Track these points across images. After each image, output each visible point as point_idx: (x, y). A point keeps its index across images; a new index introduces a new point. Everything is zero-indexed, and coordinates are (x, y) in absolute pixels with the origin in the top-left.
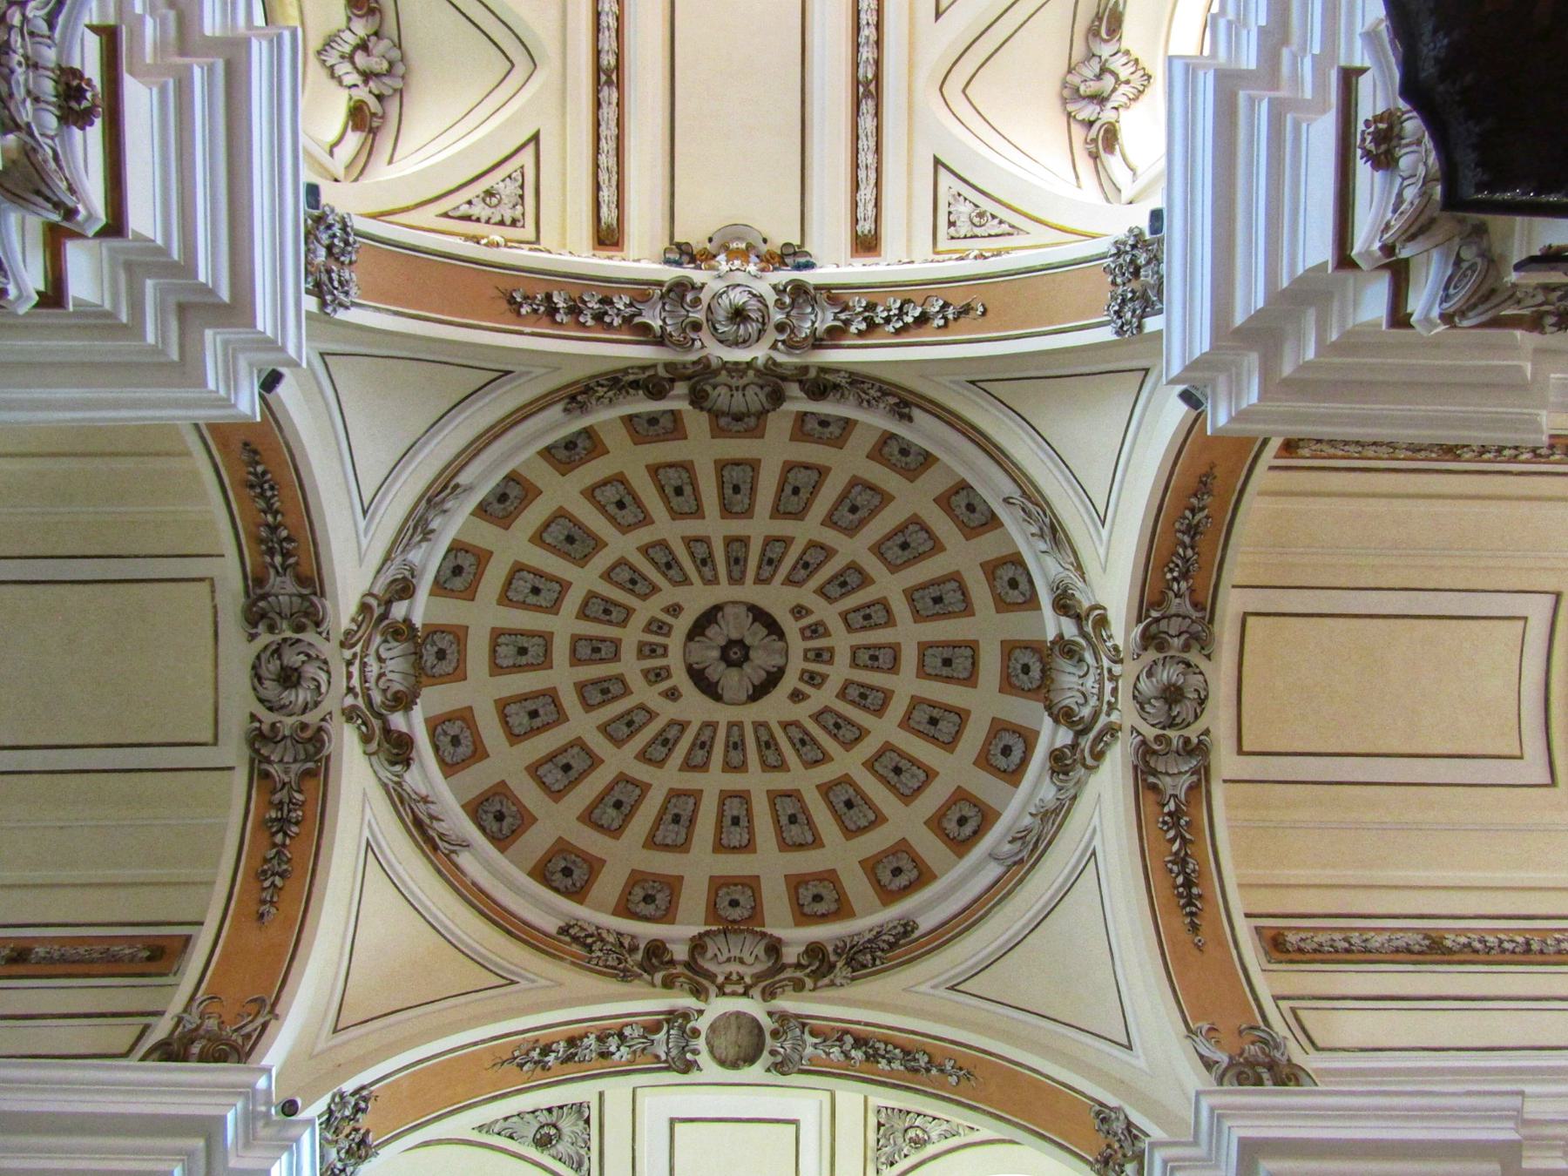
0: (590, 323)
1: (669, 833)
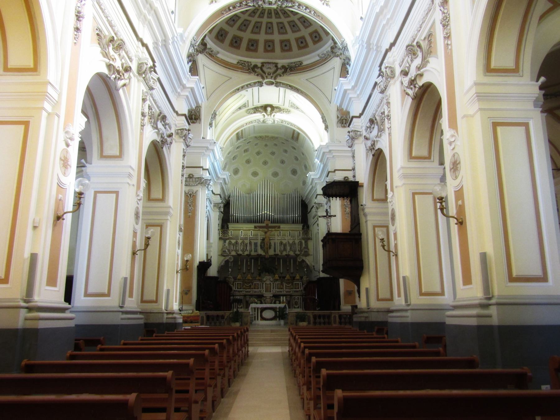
1: (256, 30)
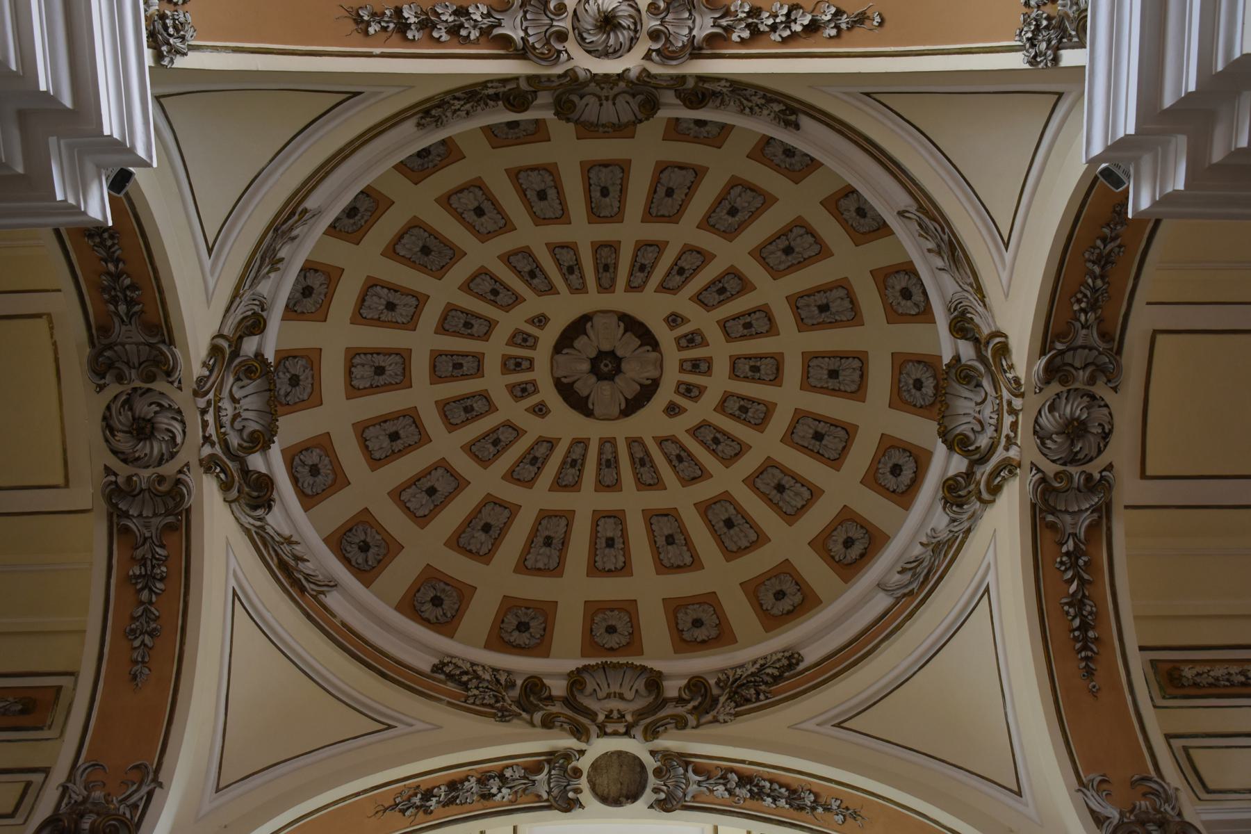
0: (445, 37)
